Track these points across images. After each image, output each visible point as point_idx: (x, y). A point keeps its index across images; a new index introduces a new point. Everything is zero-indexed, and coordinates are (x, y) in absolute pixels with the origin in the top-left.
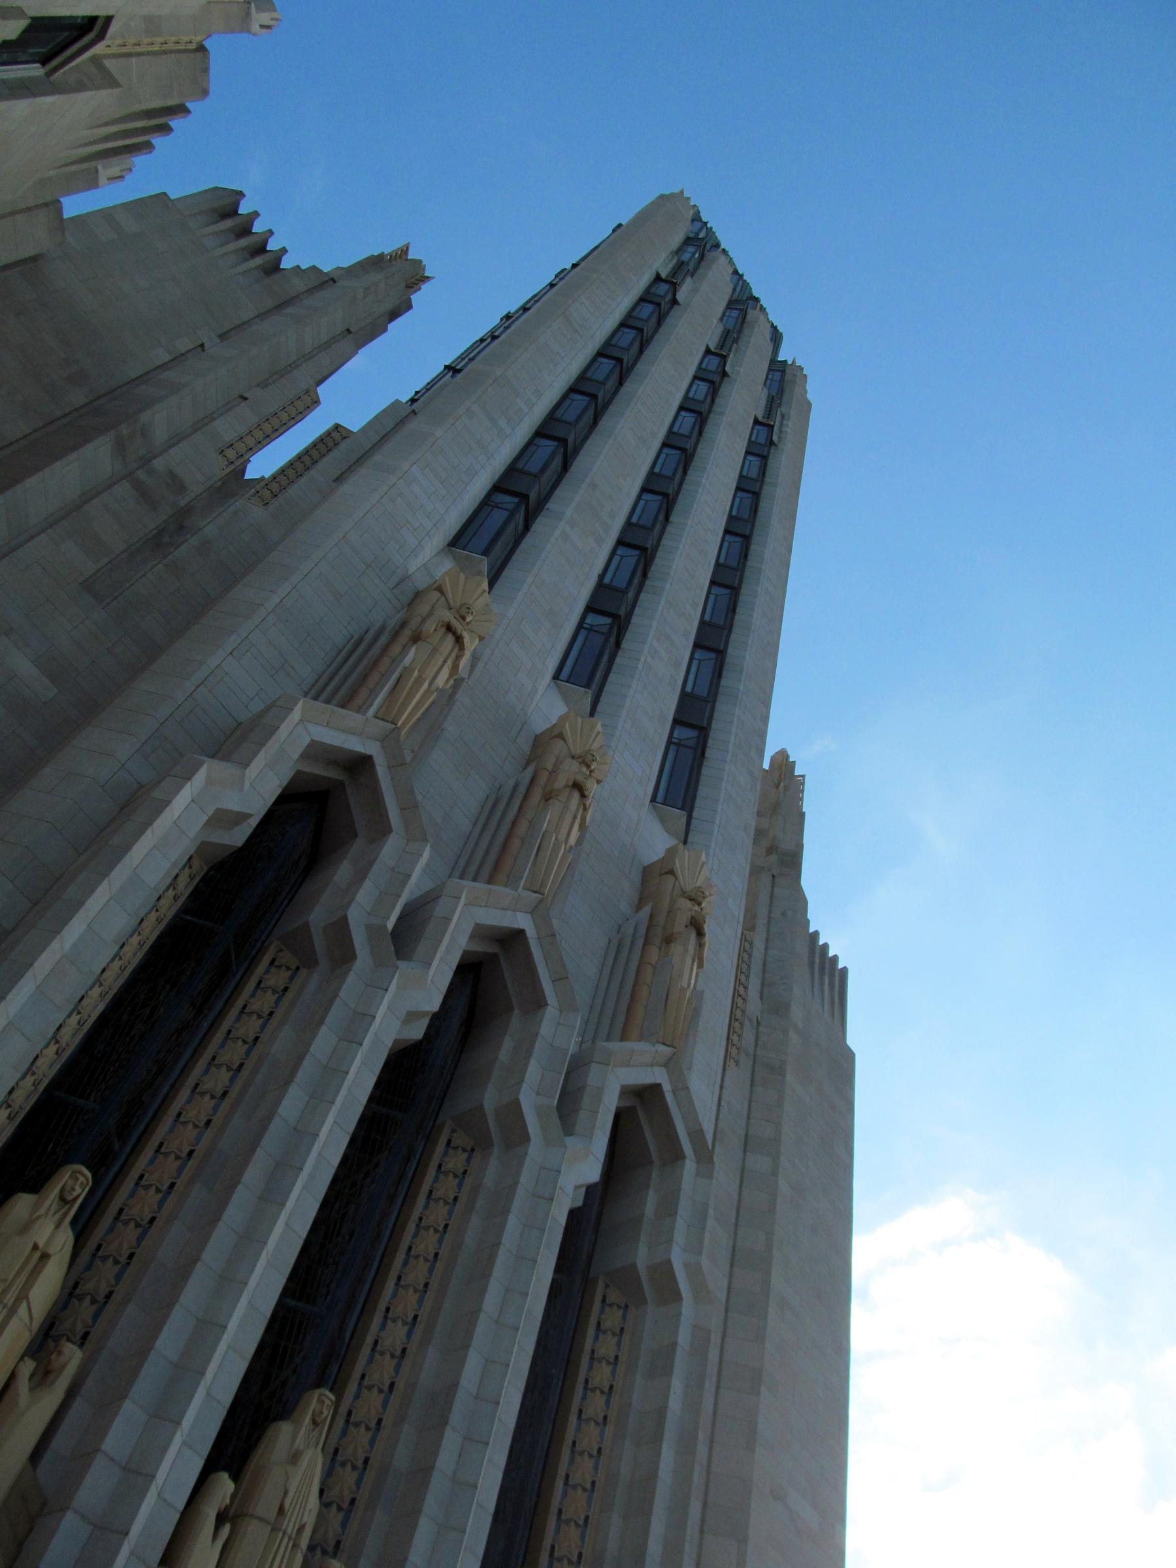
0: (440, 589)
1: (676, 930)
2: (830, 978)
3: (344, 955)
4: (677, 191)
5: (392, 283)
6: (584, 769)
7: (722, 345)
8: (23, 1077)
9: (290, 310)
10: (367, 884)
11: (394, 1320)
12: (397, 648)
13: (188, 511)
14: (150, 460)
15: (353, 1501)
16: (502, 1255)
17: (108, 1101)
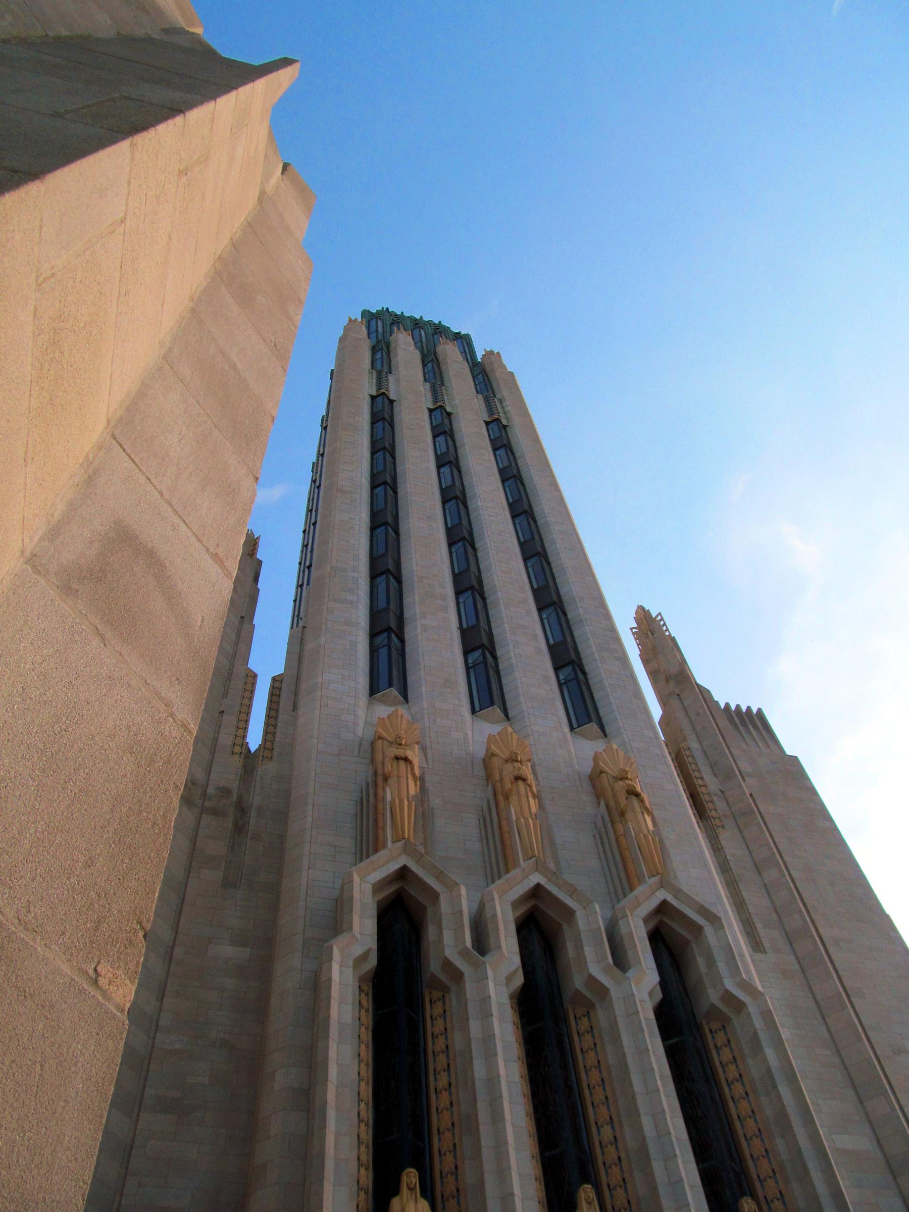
0: (380, 738)
1: (622, 806)
2: (753, 724)
3: (458, 976)
6: (516, 764)
7: (435, 400)
8: (359, 1148)
12: (380, 791)
14: (205, 792)
16: (630, 1059)
17: (406, 1126)
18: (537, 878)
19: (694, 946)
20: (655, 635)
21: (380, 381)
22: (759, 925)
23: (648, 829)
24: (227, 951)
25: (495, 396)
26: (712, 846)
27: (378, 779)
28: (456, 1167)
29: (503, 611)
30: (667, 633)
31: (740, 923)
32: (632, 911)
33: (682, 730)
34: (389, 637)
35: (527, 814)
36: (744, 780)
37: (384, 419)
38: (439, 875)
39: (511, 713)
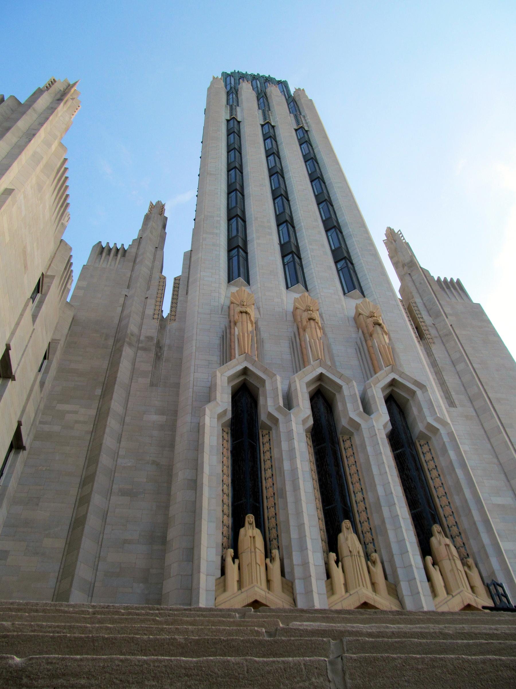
0: (232, 303)
3: (275, 421)
4: (212, 79)
5: (156, 217)
6: (309, 312)
7: (265, 119)
9: (138, 260)
10: (268, 399)
11: (357, 493)
12: (232, 330)
13: (158, 342)
15: (373, 539)
16: (371, 458)
18: (320, 370)
19: (411, 402)
20: (397, 242)
21: (232, 110)
22: (453, 393)
23: (386, 342)
24: (154, 418)
25: (301, 114)
26: (427, 353)
27: (232, 324)
28: (276, 514)
29: (305, 233)
30: (404, 241)
31: (445, 400)
32: (375, 385)
33: (411, 293)
34: (238, 252)
35: (315, 338)
36: (447, 318)
37: (234, 132)
38: (265, 371)
39: (309, 287)
